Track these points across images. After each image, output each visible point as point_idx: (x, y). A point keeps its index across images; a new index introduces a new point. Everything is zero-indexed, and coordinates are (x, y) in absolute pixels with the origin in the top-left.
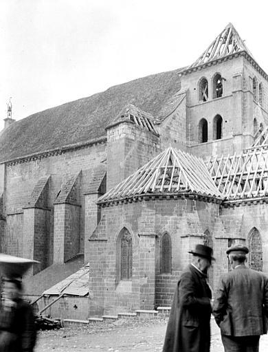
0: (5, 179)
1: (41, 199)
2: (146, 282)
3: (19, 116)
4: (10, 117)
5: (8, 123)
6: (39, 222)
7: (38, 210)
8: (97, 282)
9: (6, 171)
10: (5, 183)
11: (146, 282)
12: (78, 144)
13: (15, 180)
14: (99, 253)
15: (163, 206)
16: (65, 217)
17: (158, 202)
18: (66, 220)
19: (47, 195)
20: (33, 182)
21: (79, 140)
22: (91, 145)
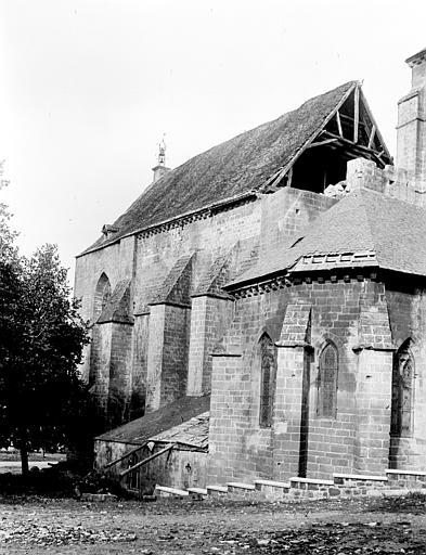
0: (135, 260)
1: (178, 290)
2: (285, 431)
3: (173, 163)
4: (162, 165)
5: (158, 174)
6: (172, 326)
7: (171, 308)
8: (222, 427)
9: (136, 247)
10: (135, 266)
11: (285, 431)
12: (235, 197)
13: (149, 260)
14: (228, 378)
15: (326, 294)
16: (207, 317)
17: (316, 287)
18: (207, 323)
19: (188, 283)
20: (171, 263)
21: (94, 246)
22: (148, 231)
